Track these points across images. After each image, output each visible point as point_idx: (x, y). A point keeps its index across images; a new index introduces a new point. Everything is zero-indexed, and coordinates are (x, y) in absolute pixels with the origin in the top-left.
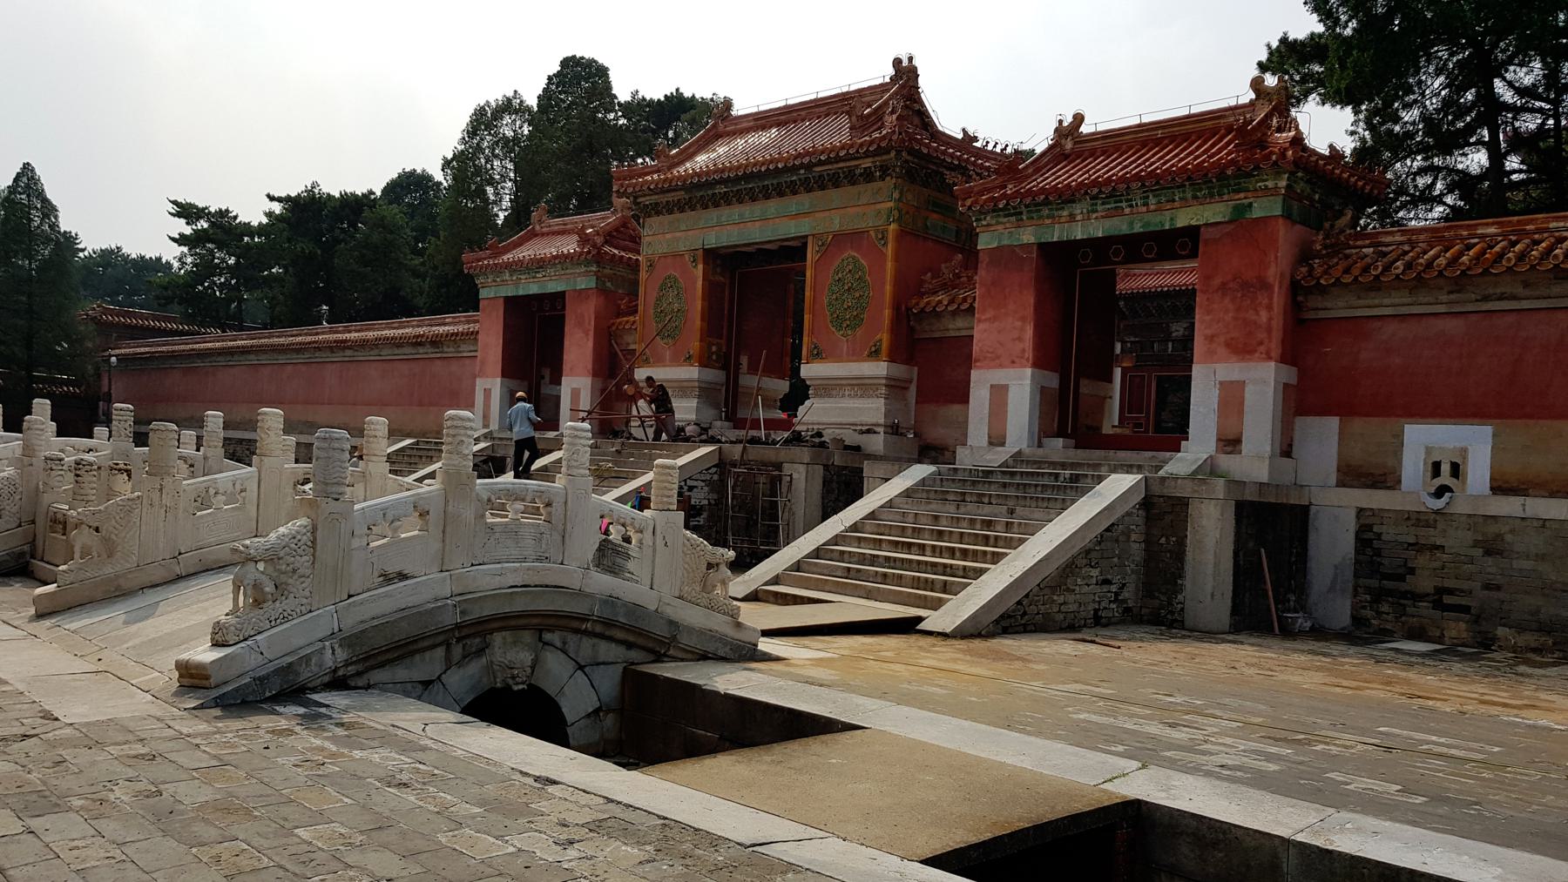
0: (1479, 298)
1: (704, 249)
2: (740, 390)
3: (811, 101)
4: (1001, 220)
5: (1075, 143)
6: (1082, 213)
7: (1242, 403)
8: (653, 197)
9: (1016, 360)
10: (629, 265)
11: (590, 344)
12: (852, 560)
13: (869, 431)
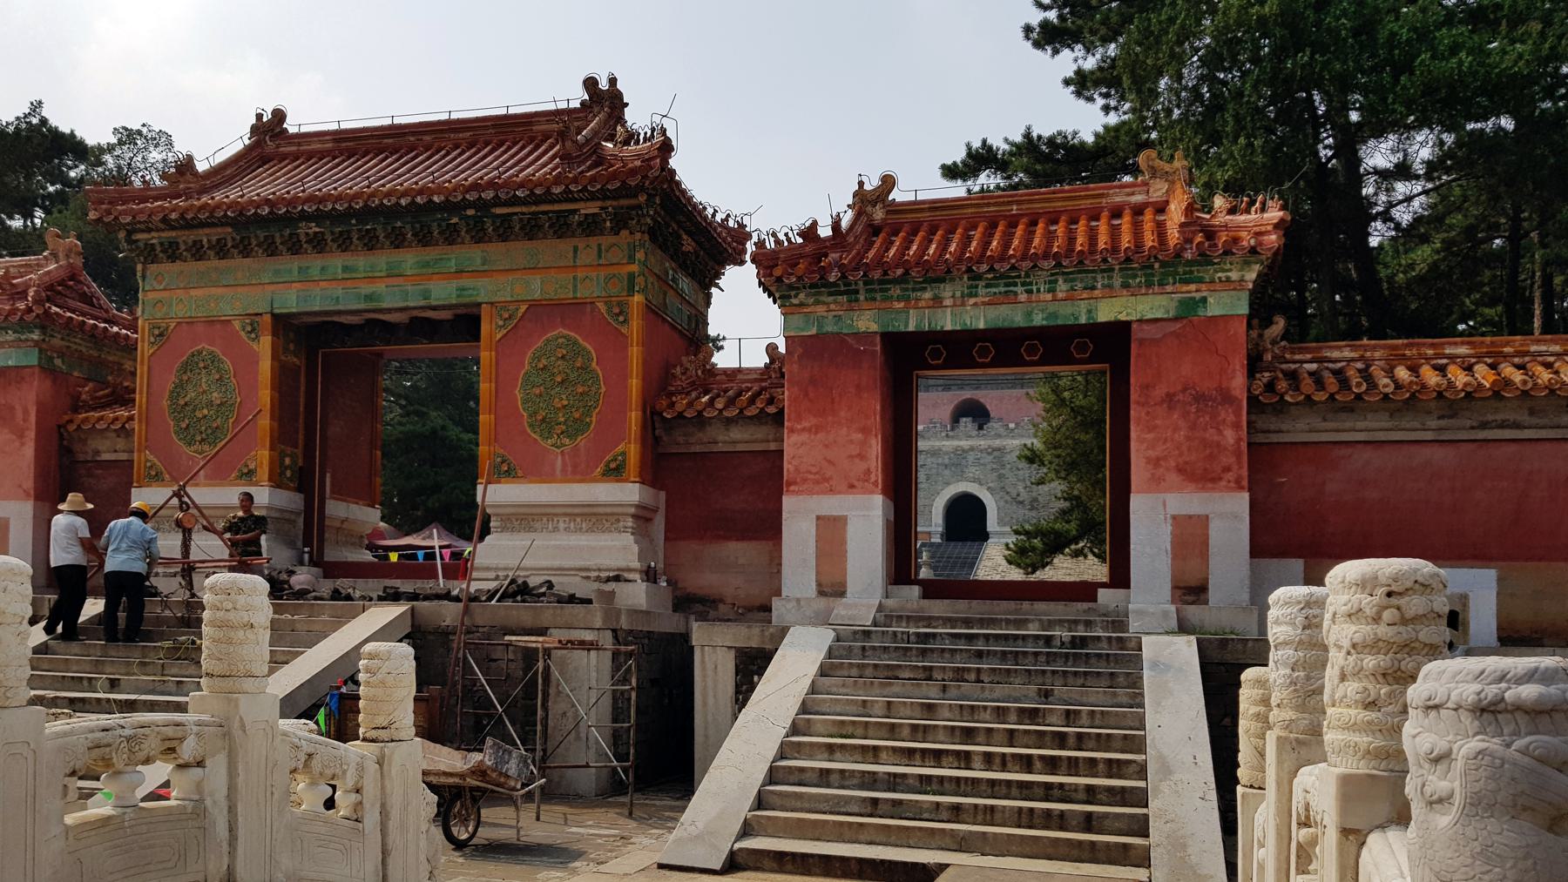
0: (1474, 424)
1: (273, 315)
2: (327, 522)
3: (439, 123)
4: (824, 298)
5: (888, 212)
6: (953, 297)
7: (1206, 543)
8: (164, 234)
9: (856, 483)
10: (93, 336)
11: (29, 451)
12: (847, 783)
13: (617, 579)
